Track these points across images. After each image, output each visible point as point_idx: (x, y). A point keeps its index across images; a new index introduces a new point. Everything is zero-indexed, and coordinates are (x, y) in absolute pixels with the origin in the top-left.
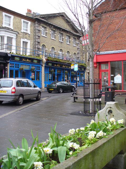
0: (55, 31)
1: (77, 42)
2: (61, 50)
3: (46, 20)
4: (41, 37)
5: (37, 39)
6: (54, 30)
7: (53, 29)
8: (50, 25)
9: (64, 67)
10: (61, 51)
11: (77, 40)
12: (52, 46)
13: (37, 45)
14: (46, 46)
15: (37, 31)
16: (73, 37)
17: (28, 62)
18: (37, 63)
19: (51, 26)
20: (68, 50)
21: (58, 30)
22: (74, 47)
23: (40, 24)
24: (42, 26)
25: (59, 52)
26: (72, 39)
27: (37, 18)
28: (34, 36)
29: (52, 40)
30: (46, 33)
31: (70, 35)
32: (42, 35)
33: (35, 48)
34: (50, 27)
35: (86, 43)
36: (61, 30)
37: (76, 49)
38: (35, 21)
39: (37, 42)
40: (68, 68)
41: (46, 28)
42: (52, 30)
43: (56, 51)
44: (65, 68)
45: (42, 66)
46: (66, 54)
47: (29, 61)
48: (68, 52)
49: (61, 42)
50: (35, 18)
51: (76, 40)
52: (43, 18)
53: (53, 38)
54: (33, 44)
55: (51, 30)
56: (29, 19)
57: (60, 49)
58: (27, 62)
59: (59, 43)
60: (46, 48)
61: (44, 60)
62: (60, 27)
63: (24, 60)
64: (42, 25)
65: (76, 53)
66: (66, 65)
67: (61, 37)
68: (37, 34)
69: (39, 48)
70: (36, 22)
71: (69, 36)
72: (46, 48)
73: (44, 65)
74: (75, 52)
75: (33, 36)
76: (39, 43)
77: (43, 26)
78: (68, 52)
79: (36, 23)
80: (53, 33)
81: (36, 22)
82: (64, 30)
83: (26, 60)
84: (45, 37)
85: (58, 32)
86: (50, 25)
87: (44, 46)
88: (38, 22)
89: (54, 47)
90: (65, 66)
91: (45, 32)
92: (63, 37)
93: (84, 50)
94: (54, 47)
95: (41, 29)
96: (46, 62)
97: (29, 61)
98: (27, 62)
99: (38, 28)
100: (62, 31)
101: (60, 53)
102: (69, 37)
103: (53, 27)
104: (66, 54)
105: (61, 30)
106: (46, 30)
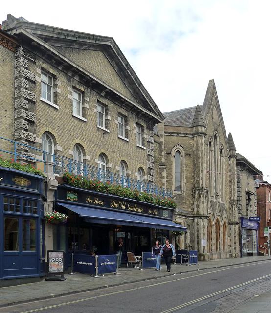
0: (83, 93)
1: (146, 136)
2: (103, 156)
3: (57, 48)
4: (39, 106)
5: (27, 110)
6: (82, 89)
7: (78, 87)
8: (69, 70)
9: (116, 206)
10: (102, 157)
11: (145, 131)
12: (77, 141)
13: (26, 130)
14: (56, 136)
15: (24, 83)
16: (137, 120)
17: (98, 205)
18: (142, 213)
19: (73, 76)
20: (123, 159)
21: (94, 92)
22: (140, 150)
23: (35, 58)
24: (42, 69)
25: (97, 161)
26: (132, 127)
27: (21, 34)
28: (15, 99)
29: (76, 122)
30: (56, 94)
31: (127, 115)
32: (42, 99)
33: (20, 139)
34: (69, 79)
35: (85, 80)
36: (103, 94)
37: (143, 155)
38: (17, 47)
39: (26, 120)
40: (126, 210)
41: (55, 77)
42: (74, 87)
43: (88, 158)
44: (118, 208)
45: (45, 200)
46: (71, 152)
47: (100, 203)
48: (122, 165)
49: (104, 132)
50: (14, 31)
51: (143, 130)
52: (47, 39)
53: (102, 126)
54: (12, 125)
55: (71, 89)
56: (8, 41)
57: (99, 153)
58: (97, 206)
59: (96, 133)
60: (56, 144)
61: (53, 179)
62: (100, 82)
63: (88, 200)
64: (43, 65)
65: (145, 168)
66: (123, 200)
67: (122, 127)
68: (24, 93)
69: (33, 140)
70: (21, 48)
71: (125, 117)
72: (56, 144)
73: (51, 198)
74: (141, 165)
75: (10, 100)
76: (31, 123)
77: (45, 72)
78: (78, 146)
79: (21, 52)
80: (103, 112)
81: (21, 48)
82: (113, 96)
83: (94, 201)
84: (51, 109)
85: (95, 99)
86: (69, 70)
87: (48, 135)
88: (27, 51)
89: (81, 146)
90: (117, 203)
91: (52, 90)
92: (109, 118)
93: (163, 160)
94: (81, 143)
95: (38, 79)
96: (58, 187)
97: (100, 203)
98: (97, 206)
99: (29, 74)
100: (105, 97)
101: (101, 164)
102: (125, 118)
103: (77, 78)
104: (118, 168)
105: (103, 94)
106: (84, 101)
